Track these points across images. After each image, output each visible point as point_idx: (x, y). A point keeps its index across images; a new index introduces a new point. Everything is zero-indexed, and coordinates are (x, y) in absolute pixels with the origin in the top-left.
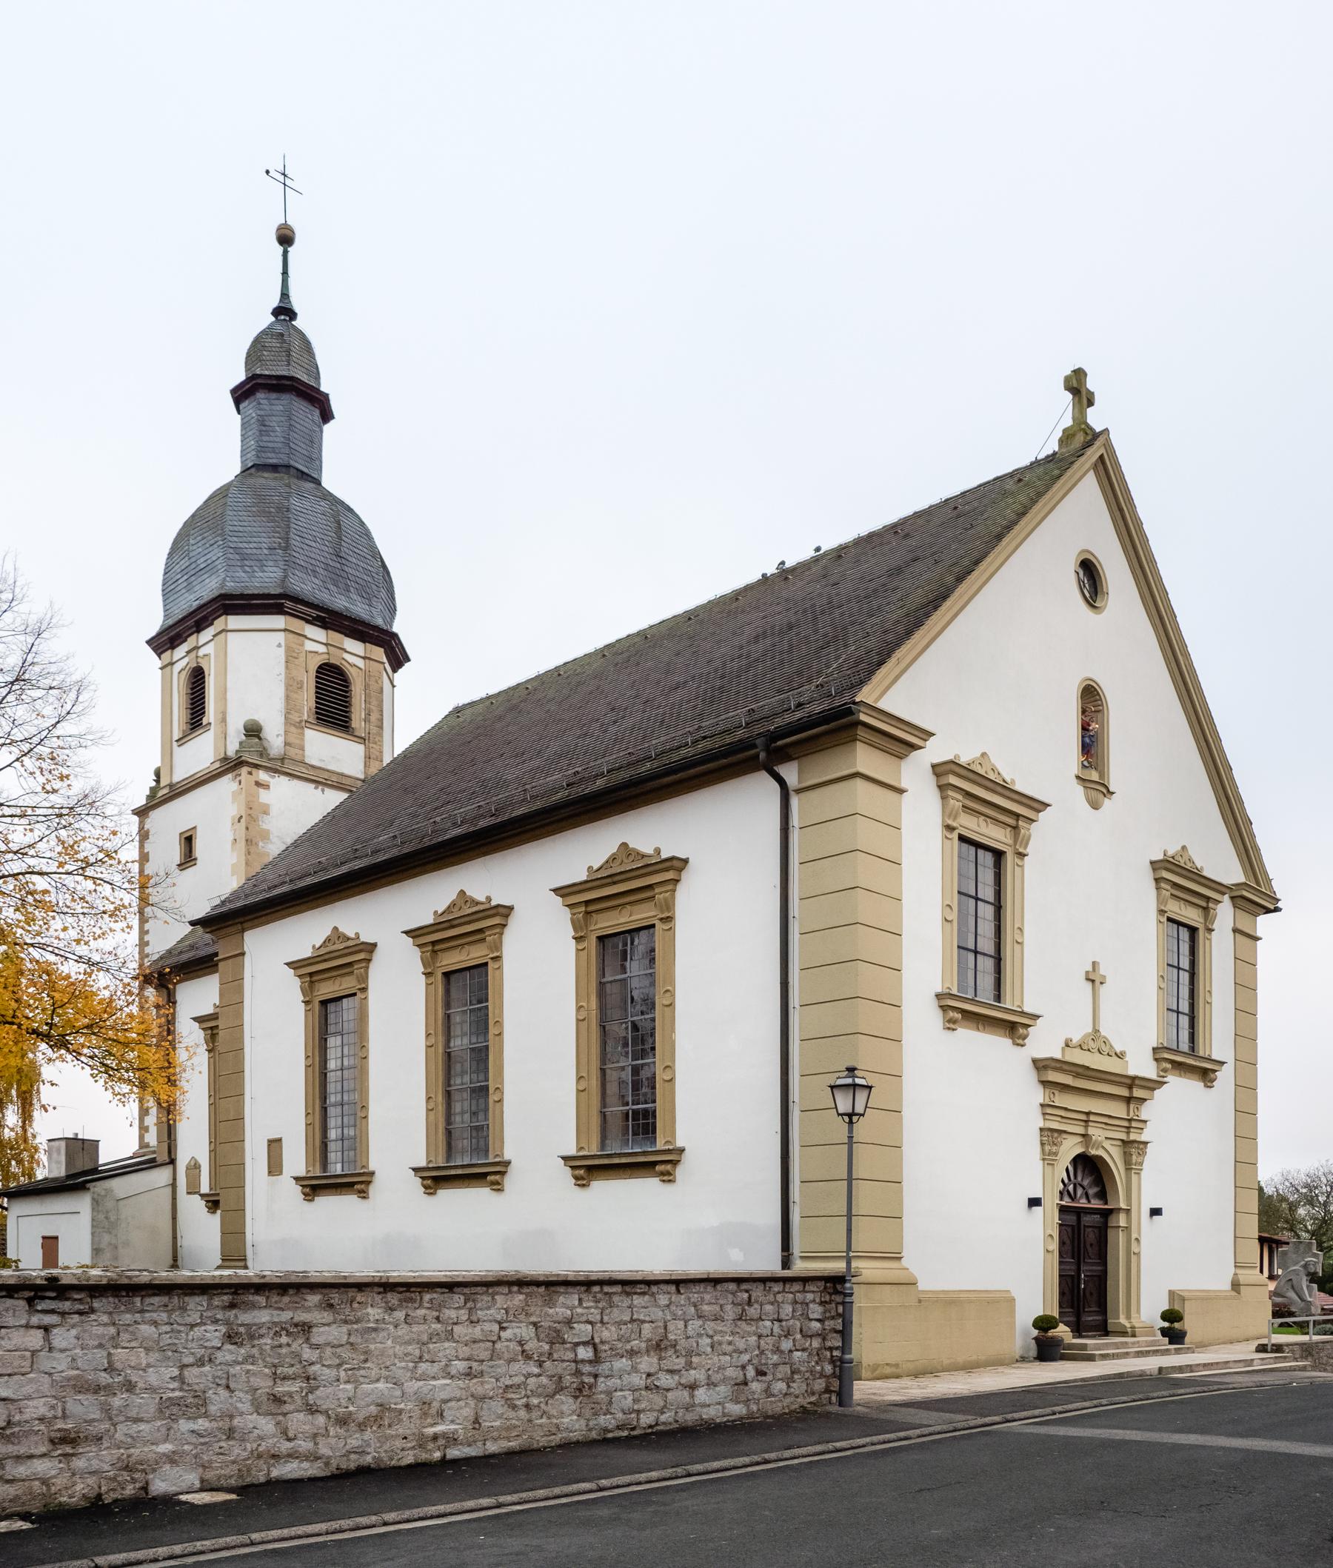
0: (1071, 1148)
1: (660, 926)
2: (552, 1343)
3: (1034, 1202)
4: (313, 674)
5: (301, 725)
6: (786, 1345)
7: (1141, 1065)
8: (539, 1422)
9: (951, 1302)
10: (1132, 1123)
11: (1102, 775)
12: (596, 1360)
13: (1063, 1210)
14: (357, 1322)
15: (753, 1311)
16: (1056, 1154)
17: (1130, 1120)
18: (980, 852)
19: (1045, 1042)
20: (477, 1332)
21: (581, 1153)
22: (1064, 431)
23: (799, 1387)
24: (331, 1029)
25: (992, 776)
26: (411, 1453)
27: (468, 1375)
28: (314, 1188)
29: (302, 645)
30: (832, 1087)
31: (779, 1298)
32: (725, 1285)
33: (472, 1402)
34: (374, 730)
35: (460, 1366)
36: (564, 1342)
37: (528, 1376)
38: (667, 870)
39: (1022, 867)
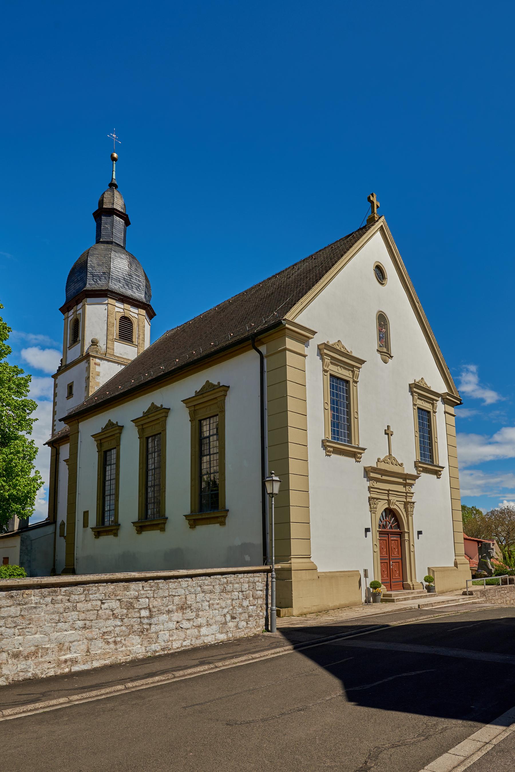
0: (382, 506)
3: (367, 530)
4: (118, 320)
6: (245, 603)
8: (121, 649)
10: (407, 494)
11: (388, 350)
12: (151, 617)
13: (381, 533)
14: (26, 604)
15: (229, 588)
16: (376, 508)
17: (406, 493)
19: (369, 460)
20: (89, 606)
24: (108, 463)
25: (343, 350)
26: (52, 670)
27: (84, 628)
28: (98, 533)
29: (114, 309)
31: (242, 580)
33: (85, 641)
34: (141, 342)
35: (80, 623)
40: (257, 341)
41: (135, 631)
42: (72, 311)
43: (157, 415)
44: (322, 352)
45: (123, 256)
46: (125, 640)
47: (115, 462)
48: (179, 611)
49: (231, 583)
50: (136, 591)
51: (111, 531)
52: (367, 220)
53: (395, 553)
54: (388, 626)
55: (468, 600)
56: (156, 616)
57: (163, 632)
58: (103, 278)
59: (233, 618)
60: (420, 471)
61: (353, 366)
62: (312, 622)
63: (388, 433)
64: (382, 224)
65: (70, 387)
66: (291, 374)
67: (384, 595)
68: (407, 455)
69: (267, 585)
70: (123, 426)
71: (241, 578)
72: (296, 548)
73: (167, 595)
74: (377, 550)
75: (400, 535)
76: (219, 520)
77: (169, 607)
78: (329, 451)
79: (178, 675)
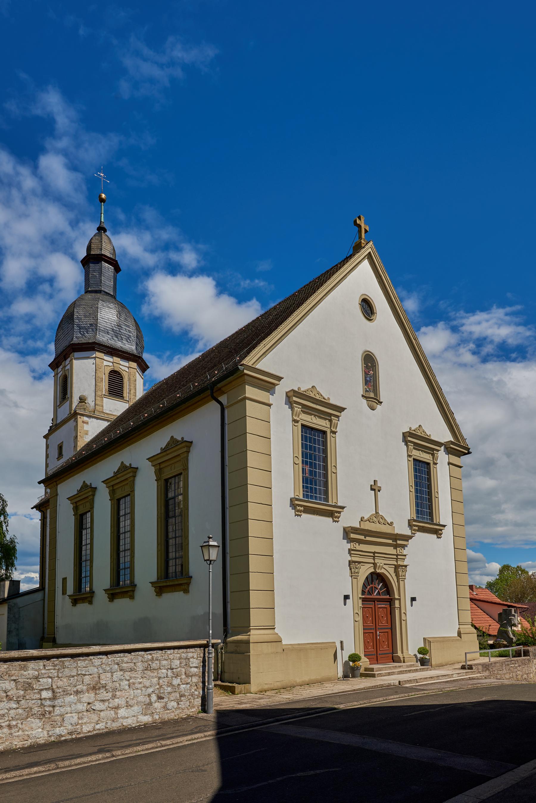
0: (365, 571)
3: (346, 597)
4: (107, 375)
6: (176, 682)
7: (402, 528)
12: (54, 698)
13: (364, 600)
15: (154, 665)
16: (358, 573)
17: (397, 555)
19: (350, 519)
25: (318, 397)
28: (75, 602)
29: (103, 363)
30: (201, 547)
31: (171, 657)
36: (33, 689)
37: (10, 709)
39: (335, 437)
40: (216, 391)
42: (61, 367)
43: (126, 474)
44: (291, 400)
45: (111, 306)
46: (22, 723)
48: (91, 692)
49: (157, 660)
50: (36, 670)
51: (86, 598)
52: (354, 248)
53: (384, 622)
54: (335, 709)
55: (465, 675)
56: (61, 697)
57: (70, 715)
58: (91, 330)
59: (160, 698)
60: (415, 530)
61: (331, 415)
62: (282, 699)
63: (375, 488)
64: (370, 250)
65: (60, 448)
66: (251, 426)
67: (366, 669)
68: (398, 511)
69: (204, 661)
70: (96, 488)
71: (171, 654)
72: (256, 618)
73: (75, 674)
74: (360, 618)
75: (390, 602)
76: (183, 587)
77: (78, 687)
78: (298, 511)
79: (62, 765)
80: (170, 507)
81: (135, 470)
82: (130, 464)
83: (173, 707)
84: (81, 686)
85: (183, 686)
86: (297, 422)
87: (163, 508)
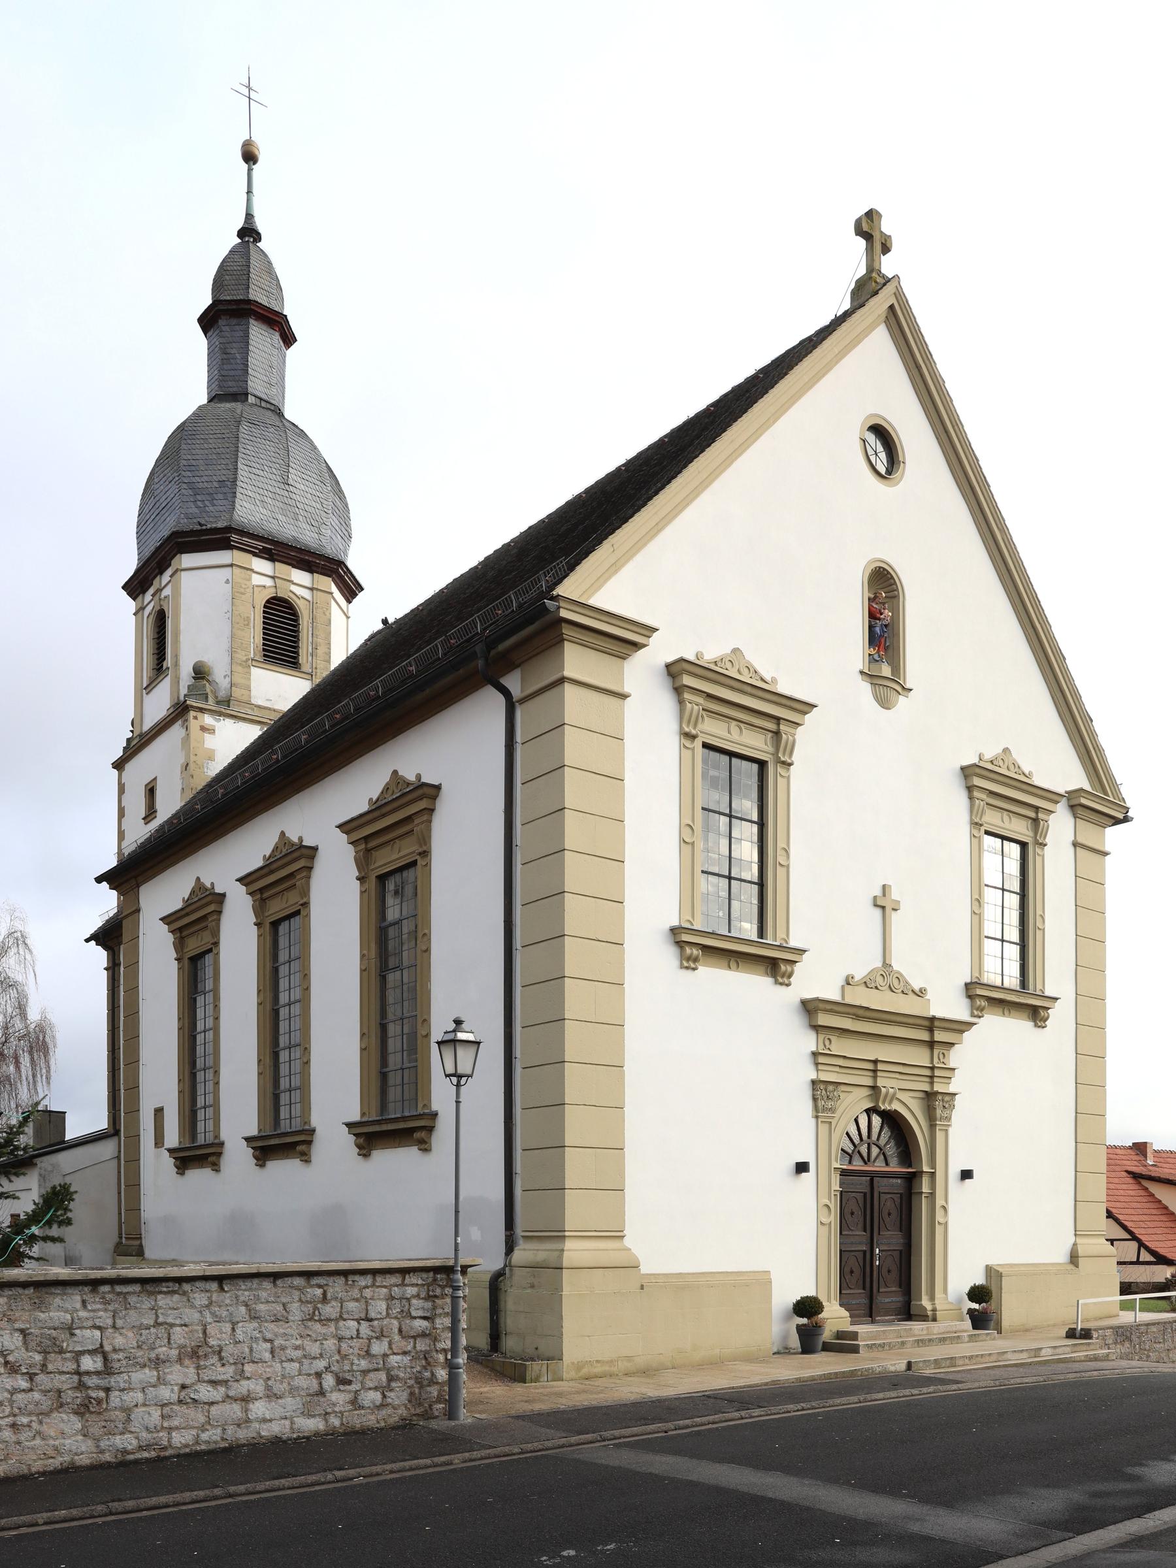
1: (420, 862)
2: (45, 1352)
3: (802, 1168)
5: (247, 664)
6: (378, 1348)
7: (947, 1003)
9: (684, 1287)
15: (330, 1310)
16: (832, 1110)
18: (734, 760)
19: (817, 978)
21: (365, 1119)
22: (857, 282)
23: (399, 1396)
29: (250, 579)
31: (368, 1293)
32: (289, 1280)
36: (61, 1351)
37: (14, 1391)
38: (420, 798)
39: (788, 778)
41: (68, 1404)
42: (151, 591)
47: (211, 987)
48: (187, 1362)
50: (66, 1311)
55: (1080, 1351)
57: (144, 1409)
58: (221, 496)
59: (342, 1381)
63: (883, 905)
65: (151, 791)
67: (840, 1335)
71: (366, 1287)
72: (577, 1211)
80: (391, 945)
81: (311, 853)
82: (301, 839)
83: (373, 1402)
84: (164, 1349)
85: (394, 1360)
86: (693, 737)
87: (373, 945)
